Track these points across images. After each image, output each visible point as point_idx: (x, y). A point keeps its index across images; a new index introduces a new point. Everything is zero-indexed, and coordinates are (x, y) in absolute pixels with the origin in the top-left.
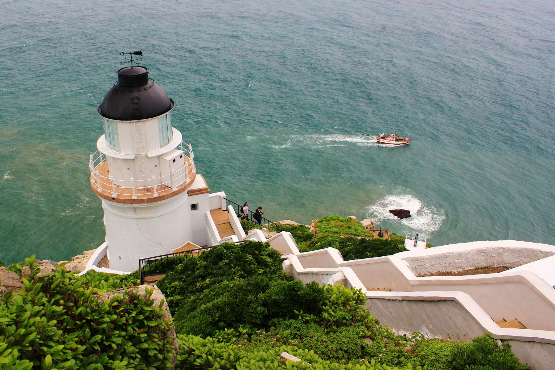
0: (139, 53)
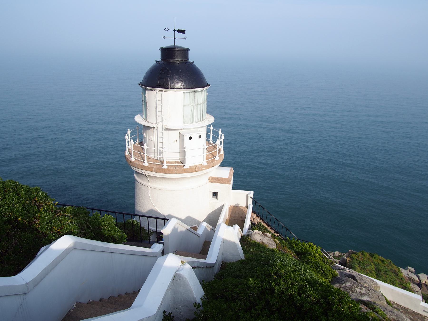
0: (183, 32)
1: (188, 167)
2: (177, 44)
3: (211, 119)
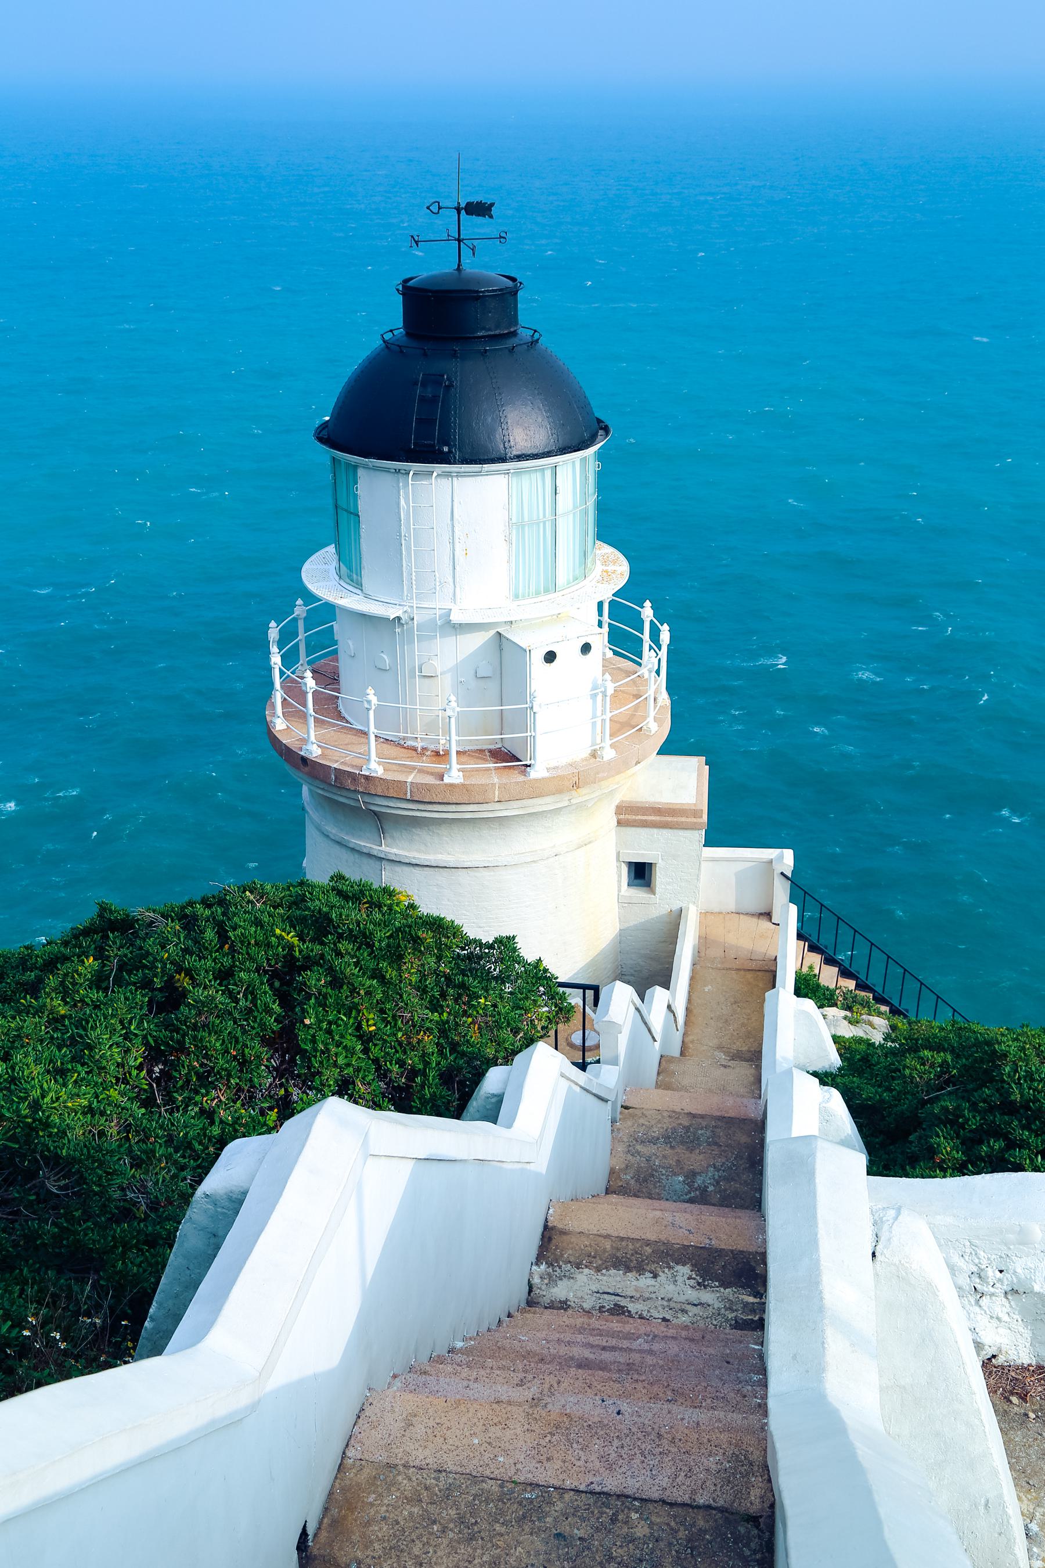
0: (479, 209)
1: (546, 774)
2: (472, 266)
3: (612, 570)
